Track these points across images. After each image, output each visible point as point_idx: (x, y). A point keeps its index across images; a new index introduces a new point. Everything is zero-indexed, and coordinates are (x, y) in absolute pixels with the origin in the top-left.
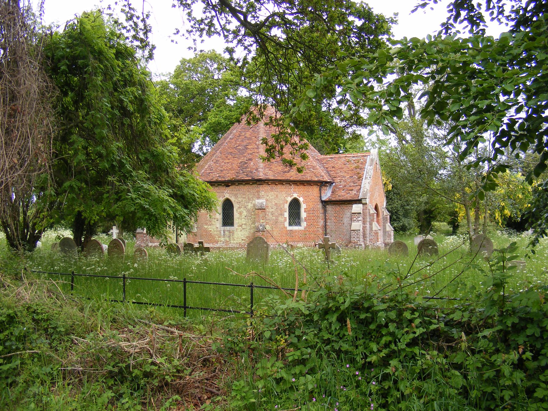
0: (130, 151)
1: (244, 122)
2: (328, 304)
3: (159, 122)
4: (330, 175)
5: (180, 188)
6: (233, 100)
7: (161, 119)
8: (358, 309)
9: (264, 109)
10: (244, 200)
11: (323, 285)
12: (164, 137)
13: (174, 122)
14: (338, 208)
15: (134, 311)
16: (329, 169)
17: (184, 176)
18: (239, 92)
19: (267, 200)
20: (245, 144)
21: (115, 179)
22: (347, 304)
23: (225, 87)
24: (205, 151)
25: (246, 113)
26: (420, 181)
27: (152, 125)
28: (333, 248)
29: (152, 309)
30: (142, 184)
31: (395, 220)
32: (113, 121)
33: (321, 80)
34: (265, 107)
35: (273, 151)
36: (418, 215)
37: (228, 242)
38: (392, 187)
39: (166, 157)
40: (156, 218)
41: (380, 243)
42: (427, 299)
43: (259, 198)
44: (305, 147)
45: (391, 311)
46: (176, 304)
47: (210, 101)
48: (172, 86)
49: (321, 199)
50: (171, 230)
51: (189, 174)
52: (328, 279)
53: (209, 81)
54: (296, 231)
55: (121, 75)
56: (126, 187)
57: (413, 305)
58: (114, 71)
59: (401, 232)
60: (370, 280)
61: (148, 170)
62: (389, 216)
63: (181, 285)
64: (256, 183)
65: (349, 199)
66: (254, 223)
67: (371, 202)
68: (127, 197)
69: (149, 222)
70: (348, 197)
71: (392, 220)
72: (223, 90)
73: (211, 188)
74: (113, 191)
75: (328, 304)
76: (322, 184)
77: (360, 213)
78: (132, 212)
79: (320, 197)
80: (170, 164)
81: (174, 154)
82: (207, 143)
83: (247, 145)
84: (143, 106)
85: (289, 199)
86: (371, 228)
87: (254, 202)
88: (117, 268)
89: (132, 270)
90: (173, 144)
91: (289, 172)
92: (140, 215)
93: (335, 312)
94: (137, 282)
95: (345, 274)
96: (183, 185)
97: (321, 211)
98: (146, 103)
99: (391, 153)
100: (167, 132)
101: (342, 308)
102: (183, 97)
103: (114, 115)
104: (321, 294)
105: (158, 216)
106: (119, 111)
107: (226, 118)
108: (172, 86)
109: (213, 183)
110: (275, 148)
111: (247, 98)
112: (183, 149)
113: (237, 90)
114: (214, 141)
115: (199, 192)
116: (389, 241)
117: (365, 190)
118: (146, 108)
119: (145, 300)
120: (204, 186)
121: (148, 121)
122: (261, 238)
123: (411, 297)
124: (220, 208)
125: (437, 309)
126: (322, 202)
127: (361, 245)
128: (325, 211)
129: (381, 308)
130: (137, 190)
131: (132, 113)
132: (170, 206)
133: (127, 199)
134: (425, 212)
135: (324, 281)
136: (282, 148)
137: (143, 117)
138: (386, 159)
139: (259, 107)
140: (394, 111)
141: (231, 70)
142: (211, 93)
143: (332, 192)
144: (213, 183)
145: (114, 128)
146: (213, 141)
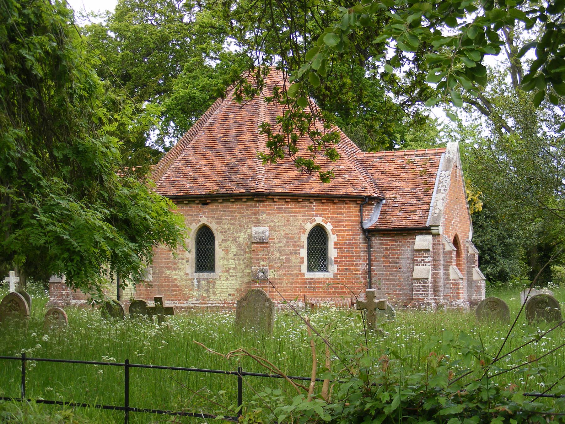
0: (37, 144)
1: (231, 95)
2: (363, 404)
3: (87, 95)
4: (377, 186)
5: (122, 207)
6: (216, 59)
7: (91, 89)
8: (414, 413)
9: (265, 74)
10: (232, 227)
11: (355, 372)
12: (97, 122)
13: (113, 96)
14: (390, 242)
15: (39, 416)
16: (376, 176)
17: (130, 187)
18: (225, 45)
19: (271, 228)
20: (234, 133)
21: (12, 190)
22: (394, 405)
23: (201, 36)
24: (168, 144)
25: (233, 81)
26: (529, 195)
27: (74, 100)
28: (382, 309)
29: (68, 412)
30: (57, 200)
31: (488, 262)
32: (8, 93)
33: (350, 18)
34: (266, 71)
35: (281, 145)
36: (528, 254)
37: (205, 298)
38: (484, 207)
39: (99, 154)
40: (82, 257)
41: (462, 301)
42: (535, 397)
43: (257, 224)
44: (334, 138)
45: (470, 417)
46: (113, 404)
47: (176, 61)
48: (112, 34)
49: (362, 226)
50: (107, 278)
51: (138, 183)
52: (365, 362)
53: (175, 25)
54: (320, 281)
55: (21, 14)
56: (30, 205)
57: (506, 408)
58: (8, 7)
59: (499, 283)
60: (435, 364)
61: (68, 176)
62: (477, 256)
63: (122, 371)
64: (252, 199)
65: (409, 226)
66: (249, 266)
67: (446, 231)
68: (33, 221)
69: (69, 264)
70: (408, 223)
71: (482, 263)
72: (197, 42)
73: (175, 208)
74: (9, 211)
75: (363, 404)
77: (428, 250)
78: (39, 248)
79: (361, 223)
80: (107, 167)
81: (113, 150)
82: (171, 131)
83: (238, 136)
84: (60, 68)
85: (309, 227)
86: (447, 276)
87: (249, 231)
88: (13, 342)
89: (39, 346)
90: (112, 134)
91: (308, 180)
92: (55, 252)
93: (374, 418)
94: (48, 366)
95: (394, 353)
96: (127, 202)
97: (363, 246)
98: (64, 63)
99: (481, 149)
100: (102, 112)
101: (387, 411)
102: (131, 54)
103: (10, 82)
104: (352, 387)
105: (85, 254)
106: (19, 76)
107: (203, 89)
108: (112, 34)
109: (178, 200)
110: (282, 140)
111: (238, 55)
112: (128, 142)
113: (222, 41)
114: (183, 128)
115: (154, 214)
116: (477, 298)
117: (437, 211)
118: (65, 72)
119: (61, 397)
120: (163, 204)
121: (68, 93)
122: (260, 292)
123: (505, 393)
124: (190, 241)
125: (549, 415)
126: (364, 231)
127: (429, 304)
128: (369, 247)
129: (453, 412)
130: (48, 210)
131: (41, 80)
132: (106, 238)
133: (32, 225)
134: (539, 248)
135: (358, 365)
136: (295, 141)
137: (59, 87)
138: (473, 159)
139: (256, 71)
140: (472, 69)
141: (209, 8)
142: (178, 47)
143: (381, 215)
144: (178, 200)
145: (10, 105)
146: (181, 128)
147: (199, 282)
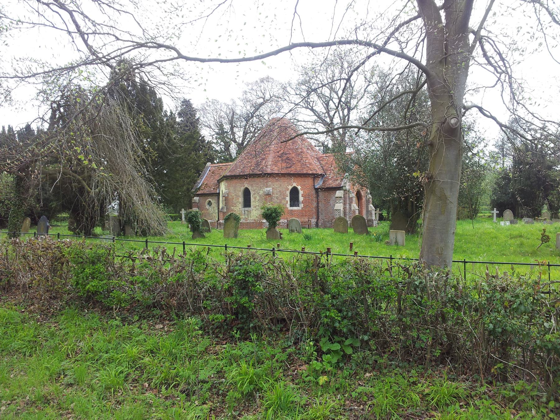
19: (273, 188)
43: (267, 187)
54: (295, 211)
76: (315, 176)
77: (341, 197)
85: (290, 188)
86: (350, 208)
128: (318, 196)
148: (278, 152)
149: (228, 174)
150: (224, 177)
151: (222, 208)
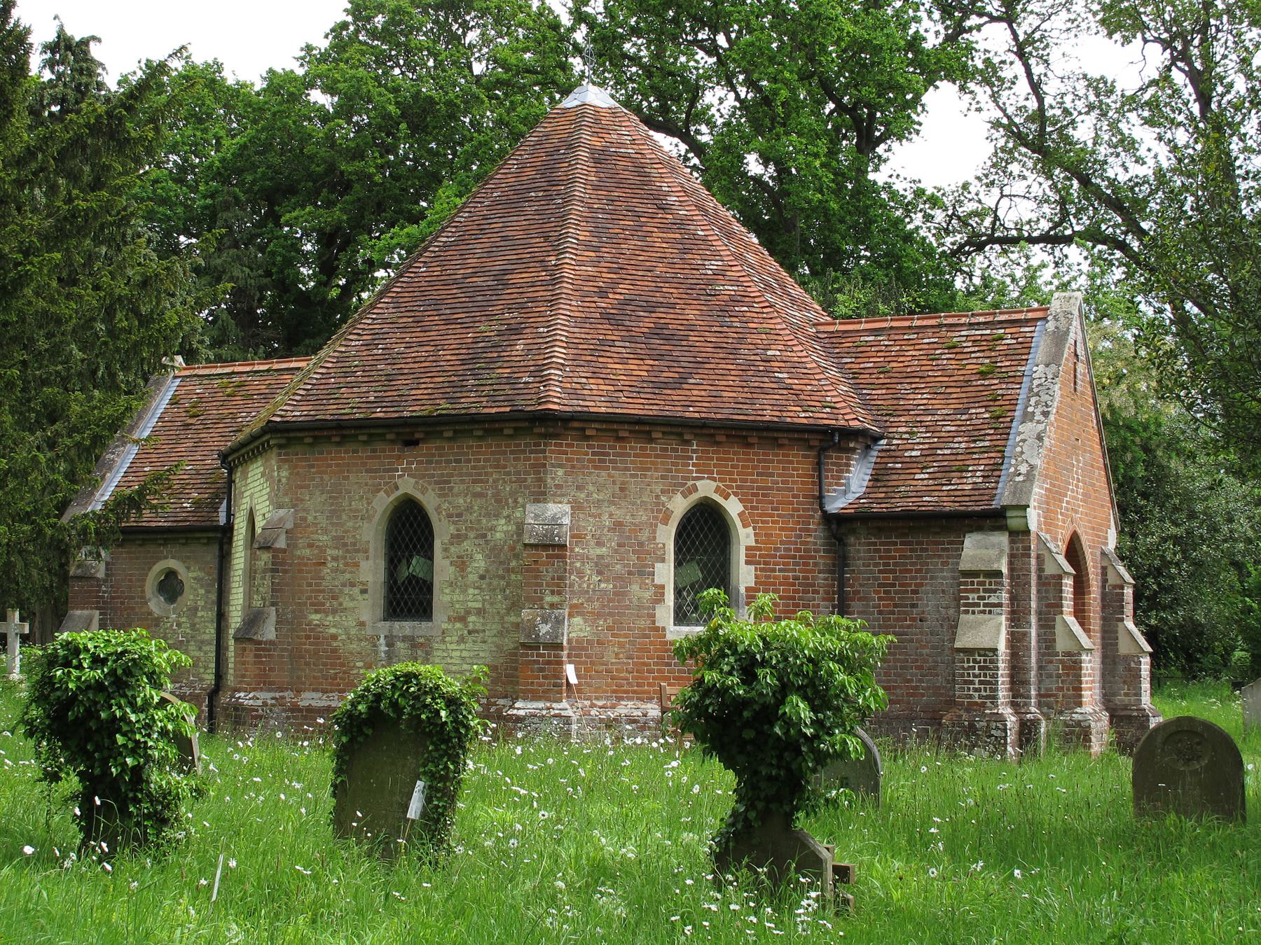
16: (865, 378)
20: (498, 266)
49: (821, 506)
65: (949, 507)
79: (820, 498)
85: (680, 506)
86: (1047, 641)
143: (875, 479)
147: (390, 644)
148: (603, 294)
149: (297, 414)
150: (271, 429)
151: (253, 619)
